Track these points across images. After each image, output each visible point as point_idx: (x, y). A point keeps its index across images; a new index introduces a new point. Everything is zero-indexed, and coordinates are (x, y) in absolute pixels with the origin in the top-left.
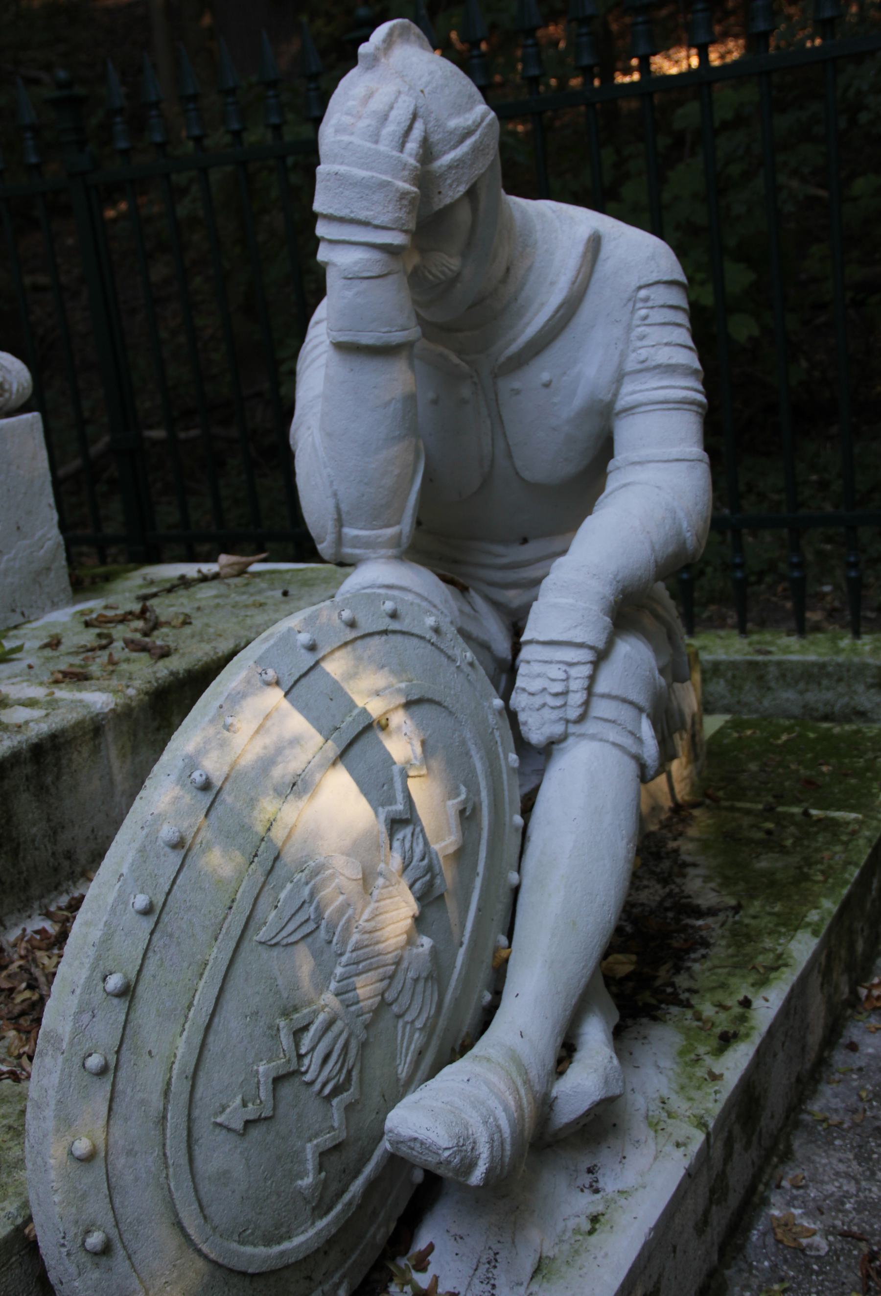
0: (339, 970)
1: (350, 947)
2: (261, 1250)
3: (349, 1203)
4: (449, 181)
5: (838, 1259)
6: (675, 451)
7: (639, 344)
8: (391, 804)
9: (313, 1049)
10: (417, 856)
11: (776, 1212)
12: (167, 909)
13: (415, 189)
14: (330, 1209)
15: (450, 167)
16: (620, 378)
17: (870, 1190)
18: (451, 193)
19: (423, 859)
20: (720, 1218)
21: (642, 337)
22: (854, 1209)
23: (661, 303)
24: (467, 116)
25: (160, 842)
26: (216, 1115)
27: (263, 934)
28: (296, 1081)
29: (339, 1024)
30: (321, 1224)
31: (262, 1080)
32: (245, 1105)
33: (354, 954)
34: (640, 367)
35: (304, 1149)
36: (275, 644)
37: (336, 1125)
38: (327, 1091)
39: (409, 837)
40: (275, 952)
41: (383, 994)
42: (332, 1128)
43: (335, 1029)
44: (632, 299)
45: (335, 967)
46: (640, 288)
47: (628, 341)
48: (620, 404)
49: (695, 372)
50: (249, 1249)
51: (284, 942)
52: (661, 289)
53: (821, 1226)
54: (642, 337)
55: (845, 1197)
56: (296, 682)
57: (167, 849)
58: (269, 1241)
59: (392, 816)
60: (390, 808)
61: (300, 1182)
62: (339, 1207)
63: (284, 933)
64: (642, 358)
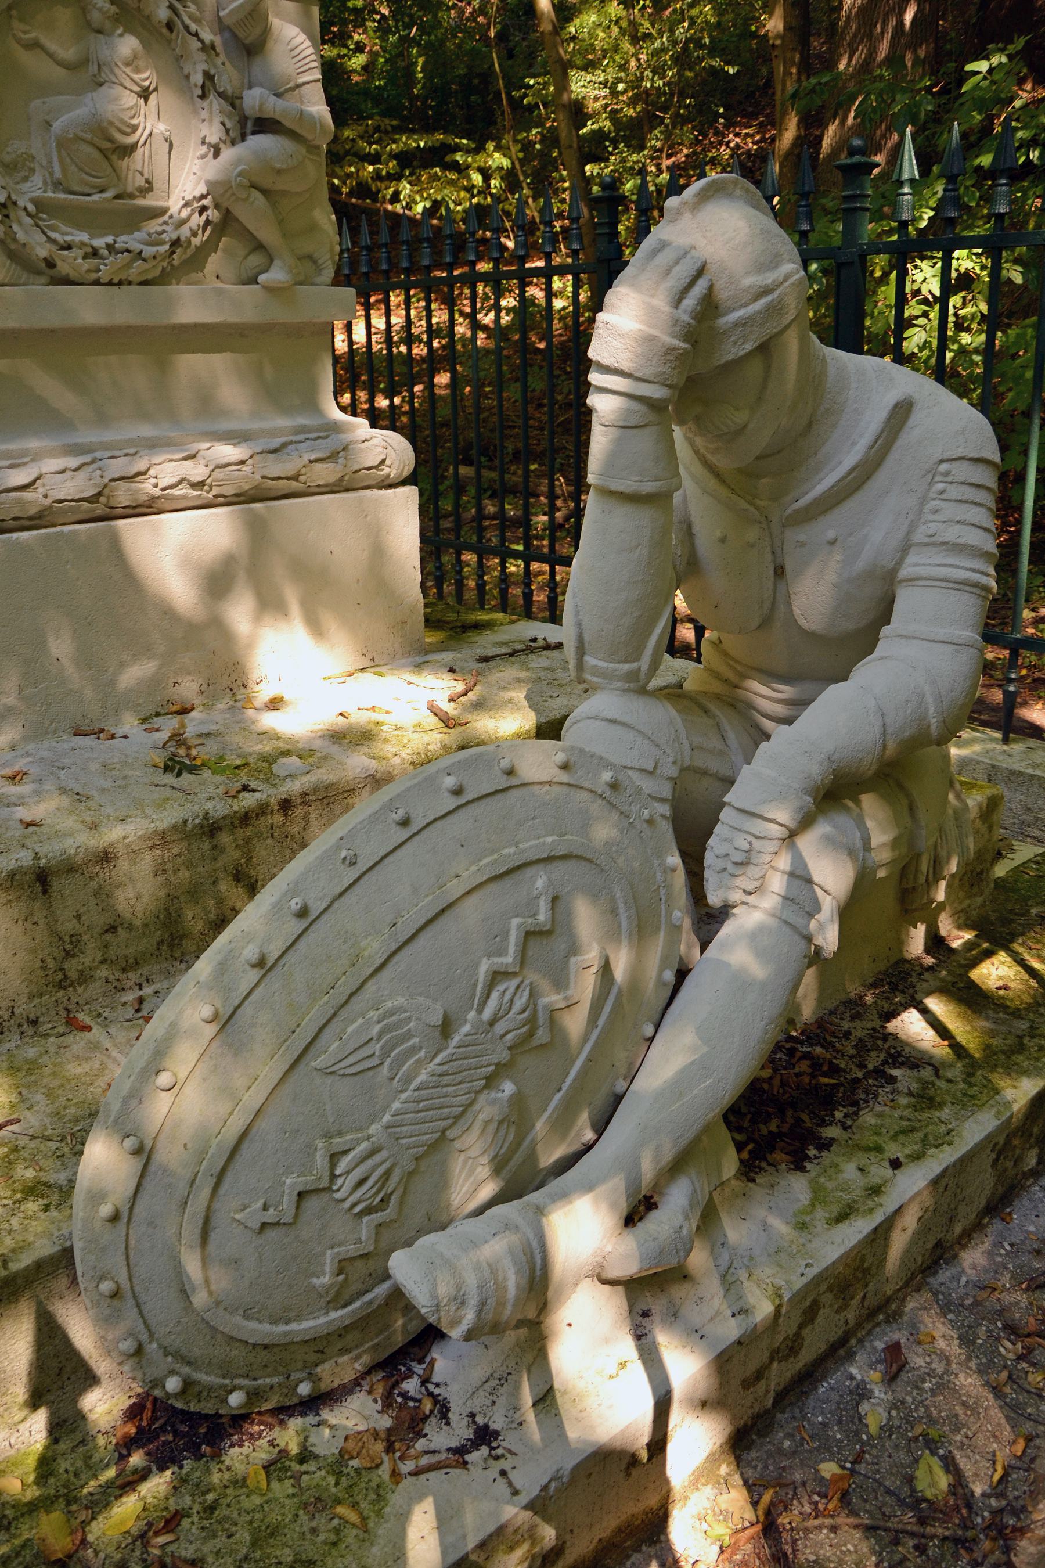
0: (396, 1105)
1: (413, 1086)
2: (267, 1327)
3: (370, 1302)
4: (733, 338)
5: (890, 1436)
6: (942, 632)
7: (932, 517)
8: (500, 956)
9: (348, 1172)
10: (518, 1004)
11: (854, 1371)
12: (232, 1021)
13: (683, 345)
14: (345, 1306)
15: (736, 325)
16: (906, 548)
17: (957, 1375)
18: (734, 350)
19: (523, 1011)
20: (780, 1374)
21: (936, 511)
22: (932, 1390)
23: (962, 479)
24: (768, 274)
25: (242, 959)
26: (236, 1212)
27: (320, 1062)
28: (325, 1197)
29: (384, 1154)
30: (334, 1315)
31: (287, 1191)
32: (265, 1208)
33: (416, 1094)
34: (927, 540)
35: (324, 1254)
36: (419, 784)
37: (363, 1239)
38: (357, 1209)
39: (512, 990)
40: (329, 1080)
41: (444, 1132)
42: (359, 1241)
43: (377, 1158)
44: (933, 472)
45: (393, 1101)
46: (942, 461)
47: (920, 512)
48: (904, 573)
49: (986, 555)
50: (253, 1325)
51: (342, 1072)
52: (965, 464)
53: (890, 1398)
54: (936, 511)
55: (929, 1375)
56: (428, 825)
57: (248, 967)
58: (275, 1322)
59: (495, 968)
60: (496, 960)
61: (315, 1280)
62: (357, 1304)
63: (342, 1064)
64: (930, 532)
